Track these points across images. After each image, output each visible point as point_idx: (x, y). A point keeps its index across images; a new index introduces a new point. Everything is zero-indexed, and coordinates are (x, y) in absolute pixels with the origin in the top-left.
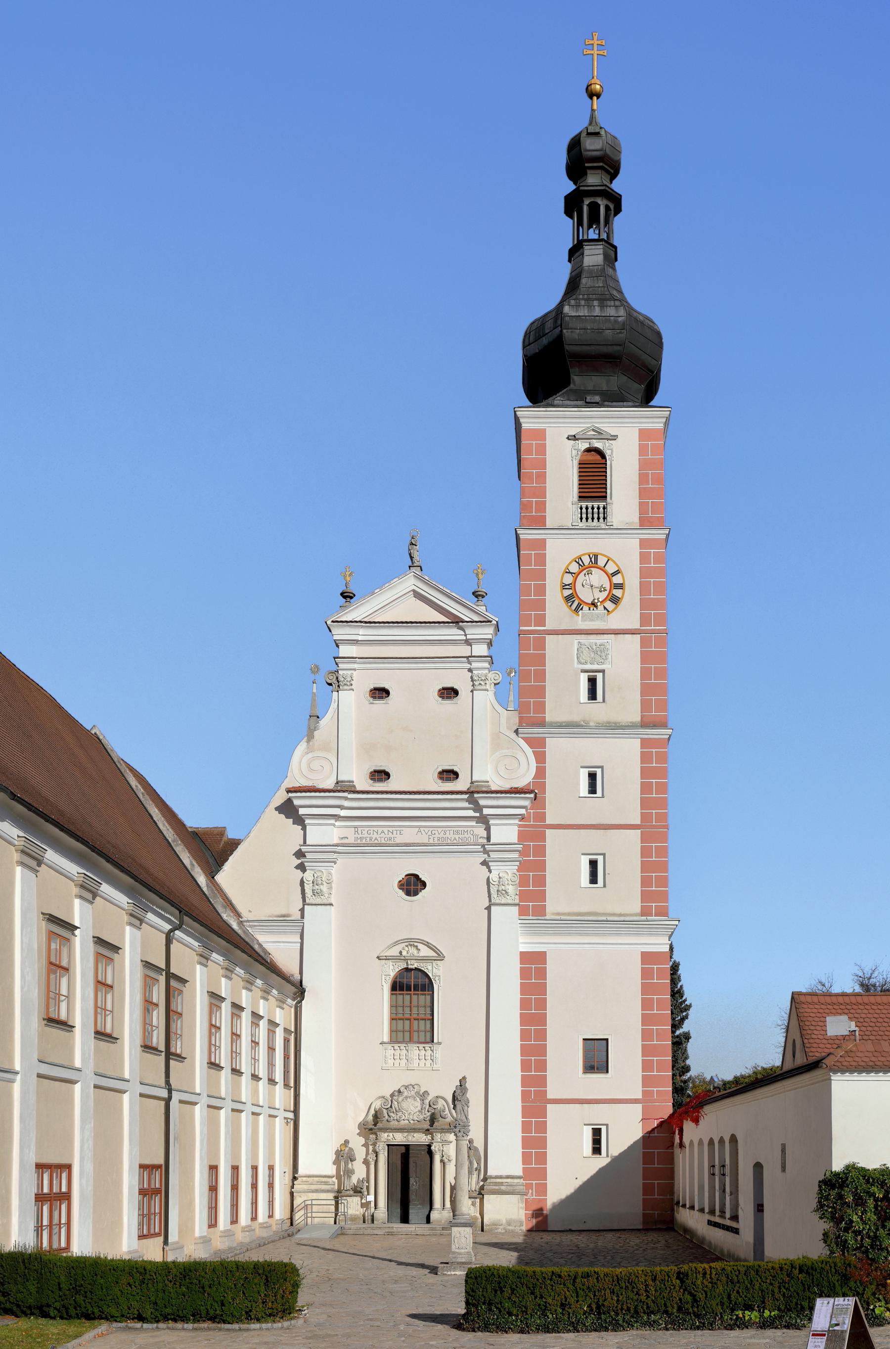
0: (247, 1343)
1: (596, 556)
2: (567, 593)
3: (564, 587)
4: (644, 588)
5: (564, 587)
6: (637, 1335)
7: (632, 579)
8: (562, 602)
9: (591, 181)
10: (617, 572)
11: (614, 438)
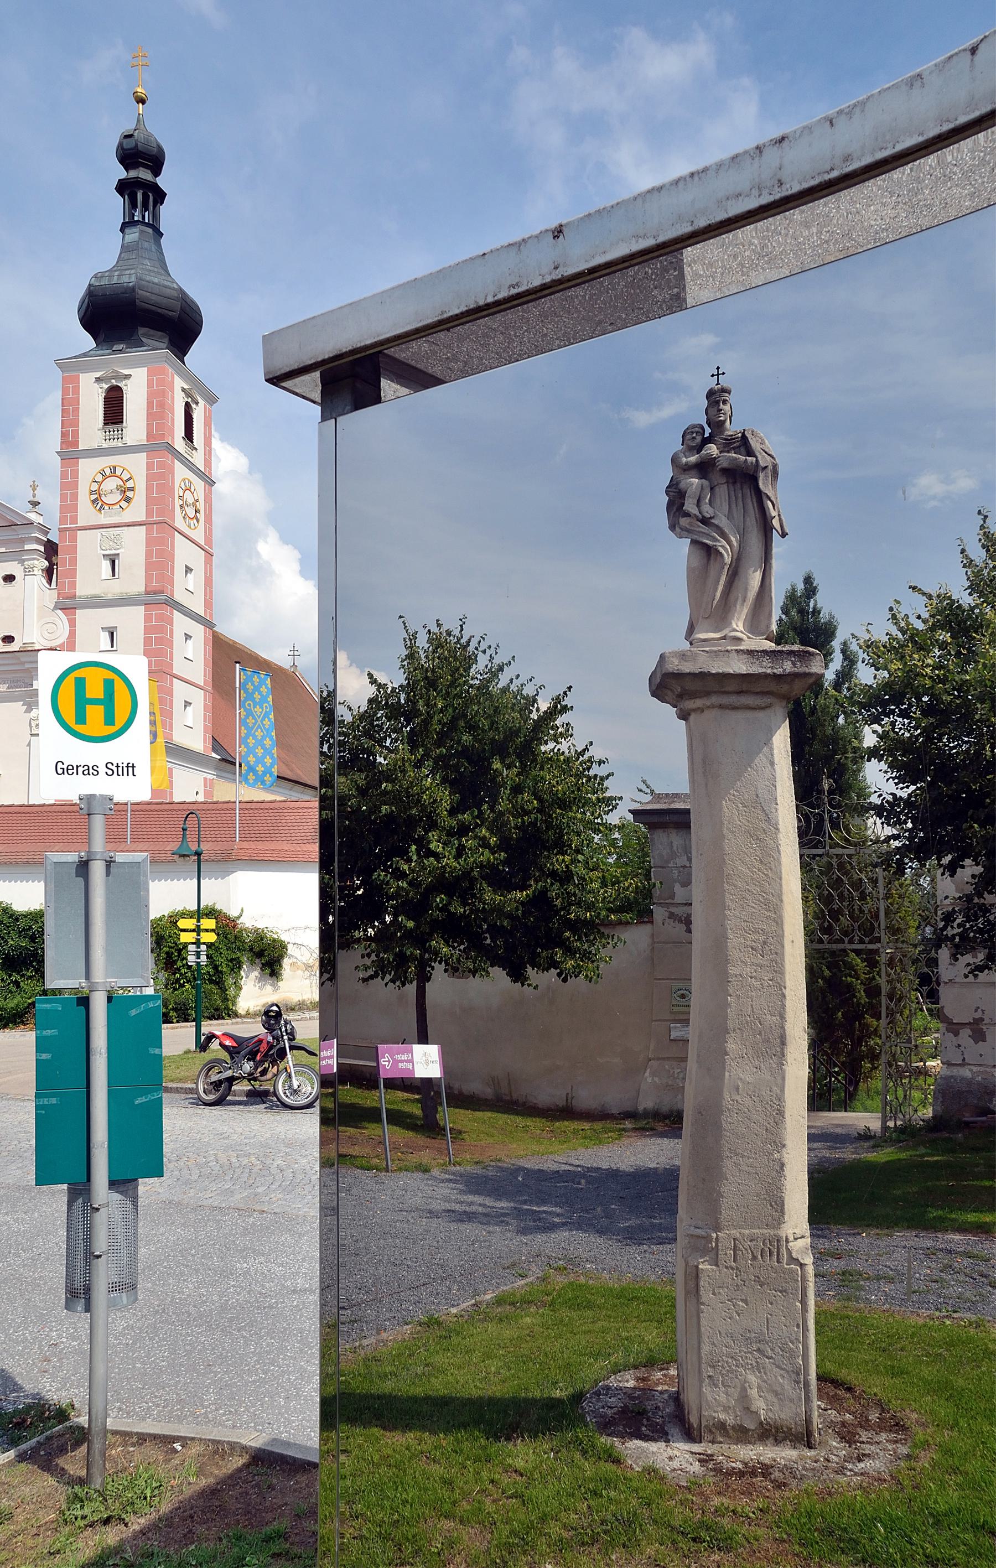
0: (523, 1276)
1: (115, 468)
2: (94, 497)
3: (92, 493)
4: (149, 488)
5: (92, 493)
6: (575, 1132)
7: (140, 483)
8: (90, 504)
9: (141, 175)
10: (130, 479)
11: (128, 377)
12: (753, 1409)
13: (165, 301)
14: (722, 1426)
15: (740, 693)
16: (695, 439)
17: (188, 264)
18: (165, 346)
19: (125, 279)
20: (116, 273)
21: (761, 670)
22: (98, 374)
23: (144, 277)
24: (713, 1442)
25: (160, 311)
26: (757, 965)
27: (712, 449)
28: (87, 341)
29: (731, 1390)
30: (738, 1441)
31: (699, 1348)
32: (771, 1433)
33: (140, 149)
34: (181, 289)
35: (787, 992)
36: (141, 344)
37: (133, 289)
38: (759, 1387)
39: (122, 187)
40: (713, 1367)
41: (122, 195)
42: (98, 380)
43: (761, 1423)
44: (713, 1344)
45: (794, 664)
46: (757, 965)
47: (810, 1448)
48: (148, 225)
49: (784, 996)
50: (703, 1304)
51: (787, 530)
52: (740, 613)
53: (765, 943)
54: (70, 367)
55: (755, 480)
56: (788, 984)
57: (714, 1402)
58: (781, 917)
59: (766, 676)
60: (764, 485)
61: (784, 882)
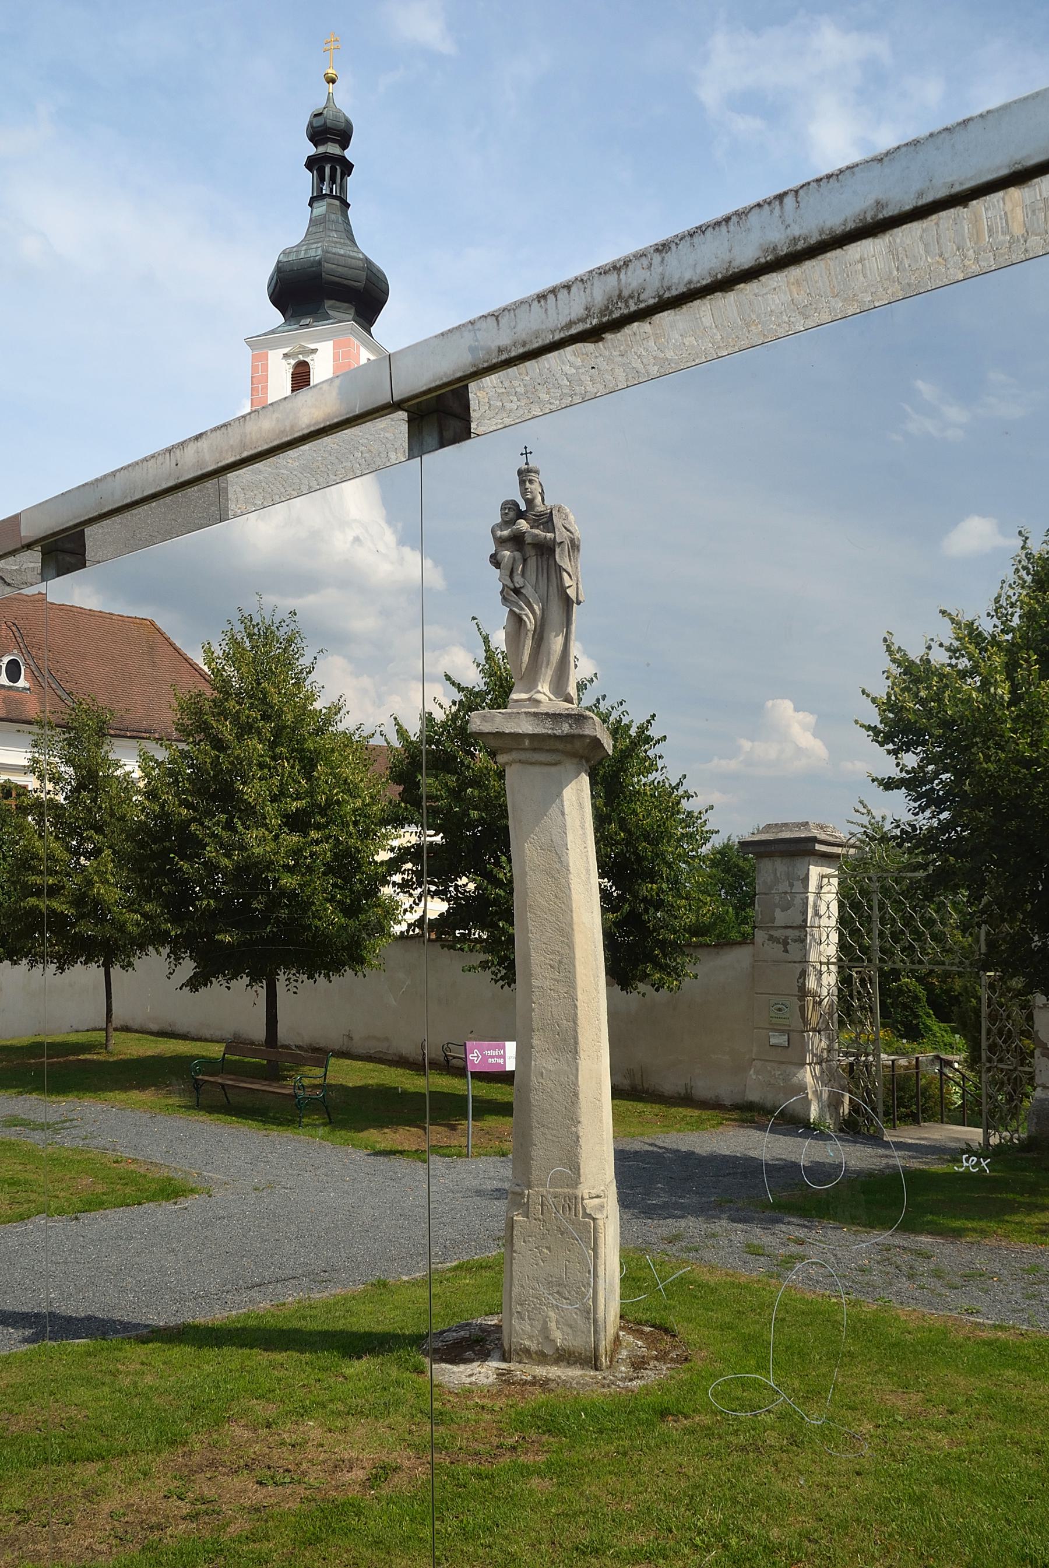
11: (314, 351)
12: (552, 1337)
13: (350, 272)
14: (527, 1351)
15: (534, 750)
16: (512, 512)
17: (375, 233)
18: (351, 317)
19: (312, 253)
20: (304, 248)
21: (544, 731)
22: (286, 350)
23: (330, 249)
24: (520, 1362)
25: (346, 282)
26: (555, 980)
27: (523, 525)
28: (277, 317)
29: (535, 1323)
30: (539, 1363)
31: (511, 1291)
32: (565, 1357)
33: (329, 125)
34: (367, 259)
35: (578, 1004)
36: (327, 317)
37: (319, 262)
38: (557, 1322)
39: (311, 163)
40: (521, 1305)
41: (311, 171)
42: (286, 356)
43: (558, 1349)
44: (522, 1286)
45: (571, 726)
46: (555, 980)
47: (597, 1370)
48: (336, 197)
49: (576, 1006)
50: (515, 1252)
51: (581, 599)
52: (545, 676)
53: (560, 962)
54: (259, 344)
55: (552, 551)
56: (580, 996)
57: (522, 1332)
58: (572, 942)
59: (549, 736)
60: (562, 559)
61: (574, 915)
